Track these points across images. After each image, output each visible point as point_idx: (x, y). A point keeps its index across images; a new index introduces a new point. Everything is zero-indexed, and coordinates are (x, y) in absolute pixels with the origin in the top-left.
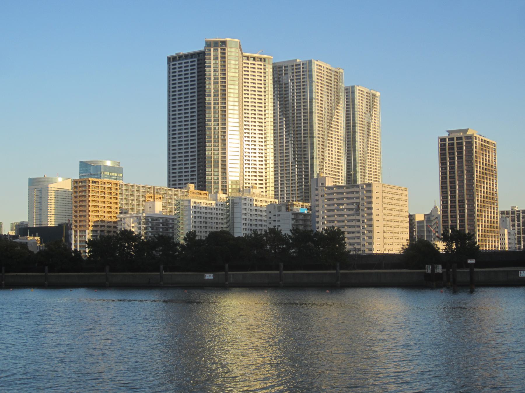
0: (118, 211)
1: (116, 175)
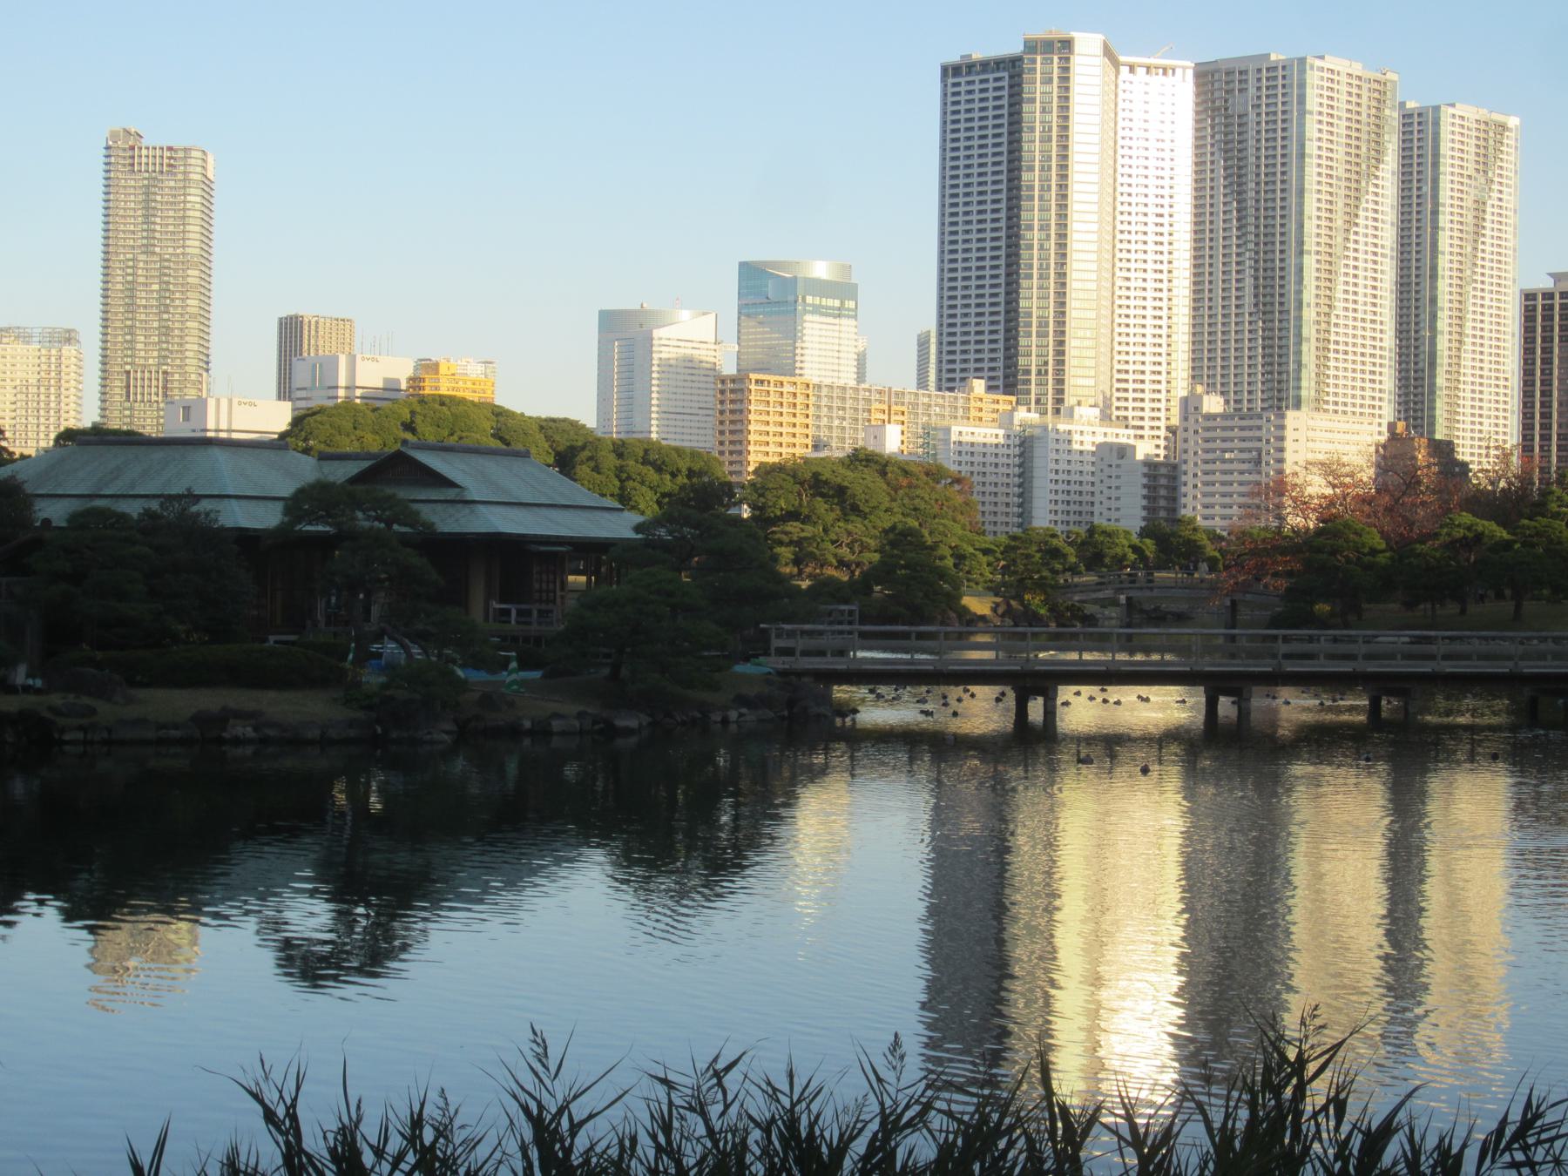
0: (809, 442)
1: (837, 303)
